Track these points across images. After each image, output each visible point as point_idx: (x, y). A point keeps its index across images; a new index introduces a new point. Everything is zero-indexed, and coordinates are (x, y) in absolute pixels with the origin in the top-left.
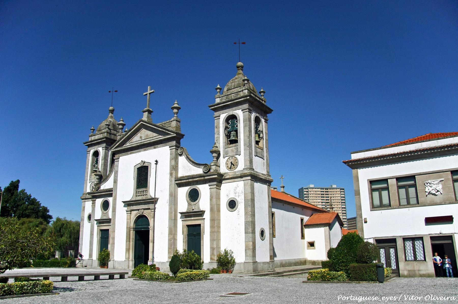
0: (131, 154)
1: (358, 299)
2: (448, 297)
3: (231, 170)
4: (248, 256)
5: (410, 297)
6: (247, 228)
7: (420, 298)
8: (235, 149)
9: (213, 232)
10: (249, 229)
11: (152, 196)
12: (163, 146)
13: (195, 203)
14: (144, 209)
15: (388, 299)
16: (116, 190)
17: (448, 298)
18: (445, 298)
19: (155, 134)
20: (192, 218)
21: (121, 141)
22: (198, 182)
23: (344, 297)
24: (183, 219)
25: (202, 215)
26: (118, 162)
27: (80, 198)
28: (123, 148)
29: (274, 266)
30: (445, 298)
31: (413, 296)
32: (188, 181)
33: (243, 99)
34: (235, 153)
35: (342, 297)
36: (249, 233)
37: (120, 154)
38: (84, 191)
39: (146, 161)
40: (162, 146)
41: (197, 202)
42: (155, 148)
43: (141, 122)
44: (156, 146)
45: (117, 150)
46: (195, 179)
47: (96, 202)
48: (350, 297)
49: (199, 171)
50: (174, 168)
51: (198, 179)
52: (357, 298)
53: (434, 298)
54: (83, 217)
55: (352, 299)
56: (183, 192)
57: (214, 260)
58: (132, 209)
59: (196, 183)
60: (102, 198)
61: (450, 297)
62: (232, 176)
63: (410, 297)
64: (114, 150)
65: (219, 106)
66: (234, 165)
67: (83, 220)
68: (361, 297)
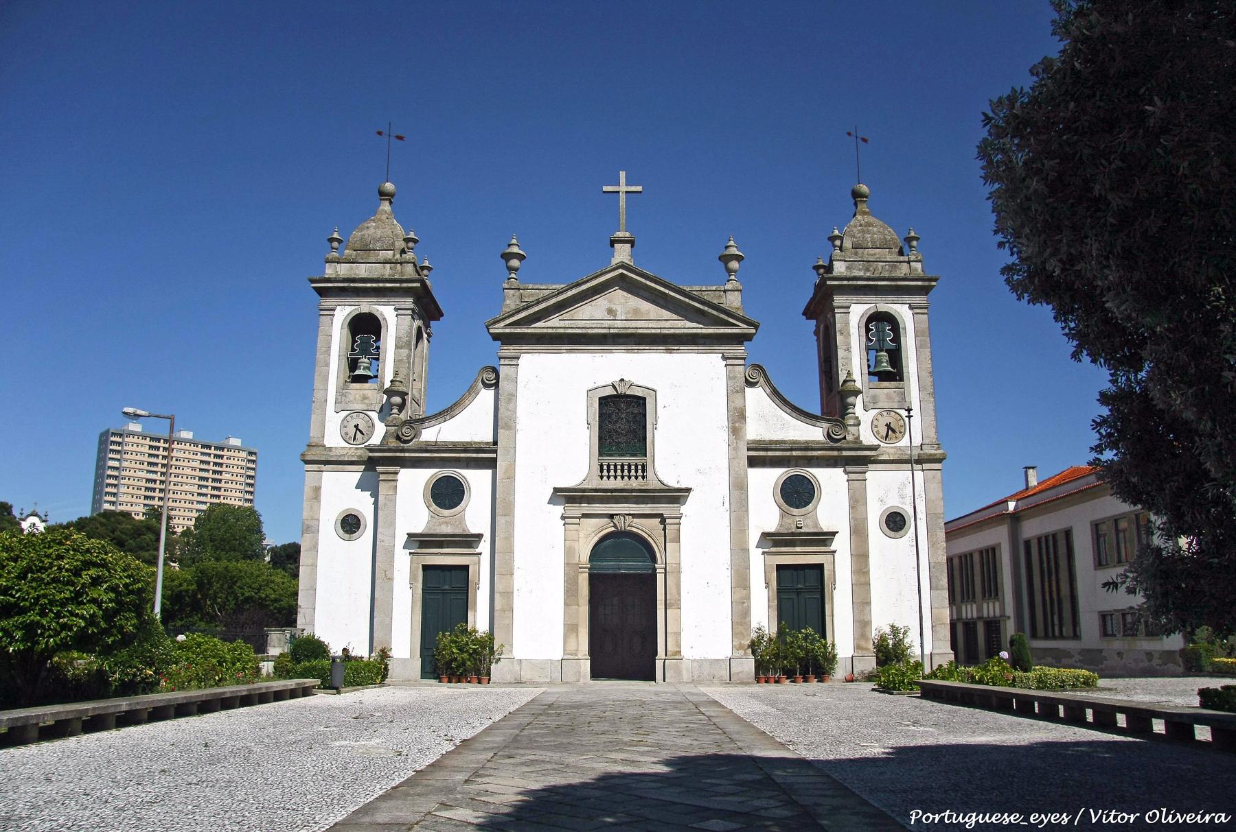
0: (569, 352)
1: (966, 819)
2: (1208, 815)
3: (887, 442)
4: (941, 640)
5: (1104, 816)
6: (937, 577)
7: (1132, 818)
8: (895, 394)
9: (860, 584)
10: (942, 579)
11: (665, 482)
12: (700, 351)
13: (803, 510)
14: (634, 516)
15: (1045, 821)
16: (512, 450)
17: (1207, 818)
18: (1199, 817)
19: (666, 314)
20: (798, 549)
21: (536, 309)
22: (811, 460)
23: (929, 814)
24: (767, 550)
25: (827, 543)
26: (513, 369)
27: (299, 457)
28: (529, 331)
29: (640, 712)
30: (1199, 817)
31: (1113, 813)
32: (788, 453)
33: (920, 283)
34: (898, 403)
35: (922, 816)
36: (943, 589)
37: (525, 347)
38: (311, 435)
39: (635, 383)
40: (696, 351)
41: (810, 510)
42: (670, 351)
43: (621, 271)
44: (676, 348)
45: (513, 330)
46: (810, 453)
47: (399, 477)
48: (943, 814)
49: (815, 433)
50: (737, 417)
51: (820, 452)
52: (963, 818)
53: (1171, 816)
54: (316, 523)
55: (948, 820)
56: (764, 482)
57: (867, 649)
58: (585, 512)
59: (806, 462)
60: (430, 468)
61: (1214, 814)
62: (896, 457)
63: (1104, 816)
64: (508, 330)
65: (855, 283)
66: (894, 431)
67: (311, 529)
68: (974, 814)
